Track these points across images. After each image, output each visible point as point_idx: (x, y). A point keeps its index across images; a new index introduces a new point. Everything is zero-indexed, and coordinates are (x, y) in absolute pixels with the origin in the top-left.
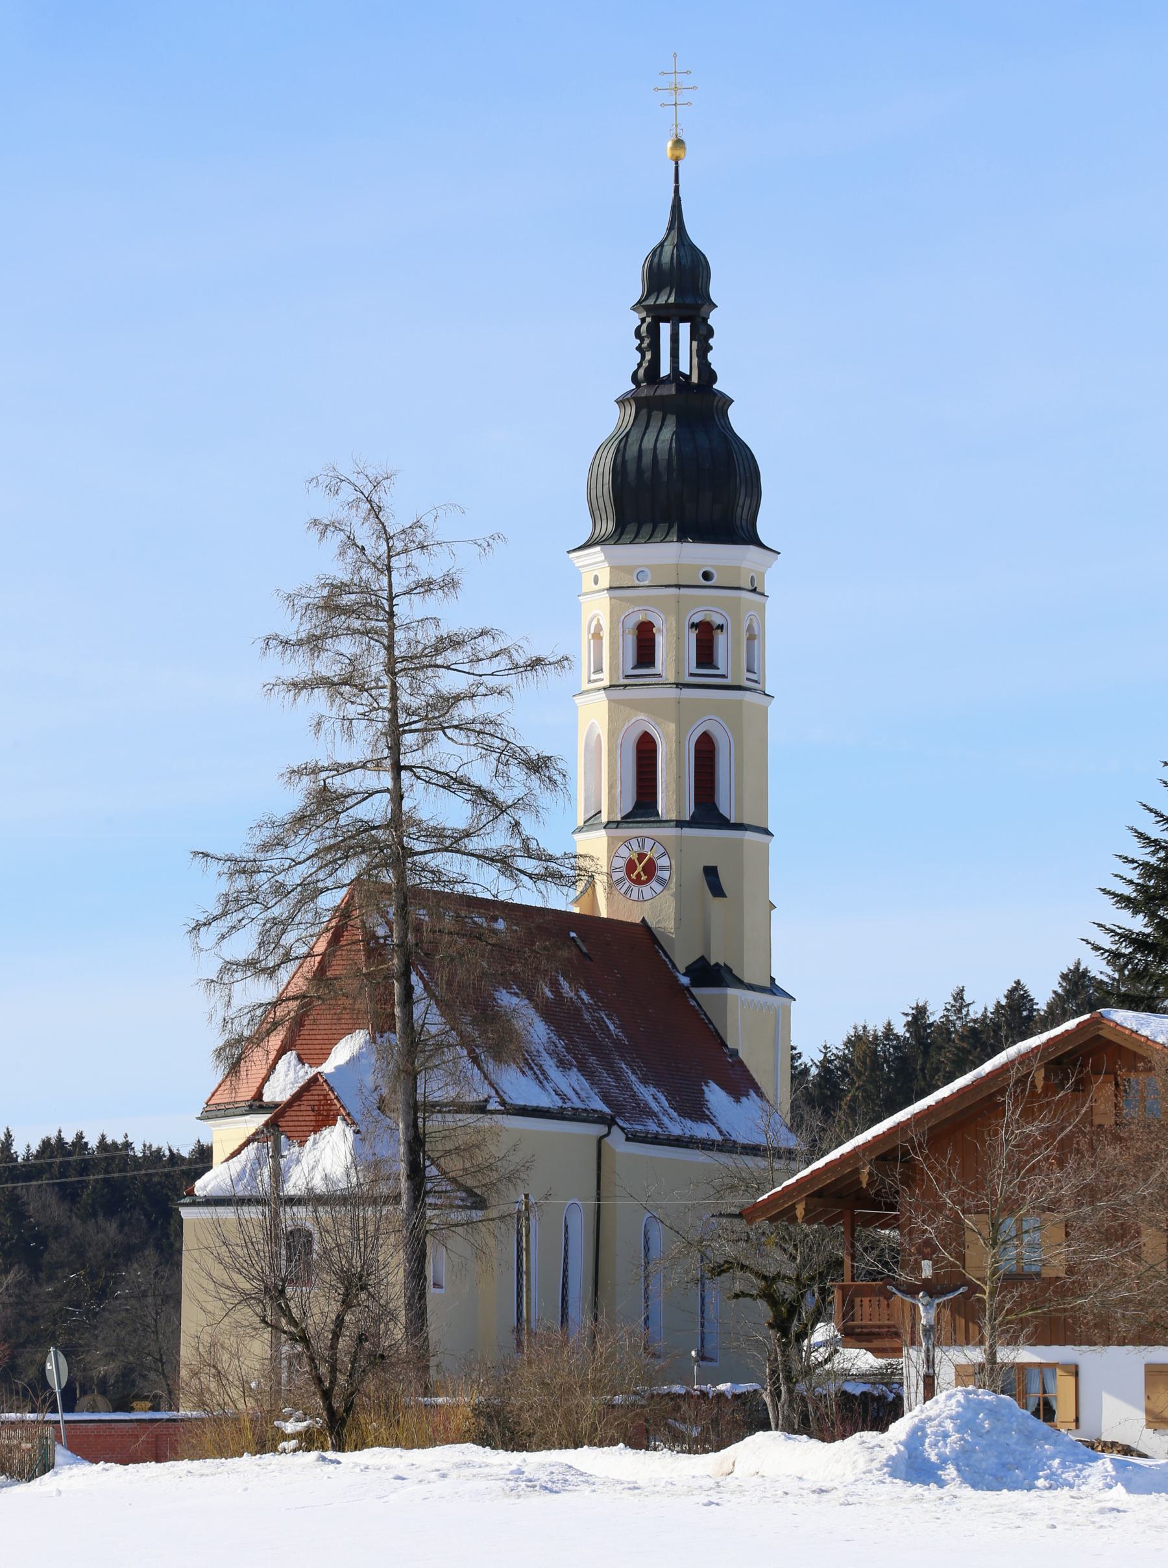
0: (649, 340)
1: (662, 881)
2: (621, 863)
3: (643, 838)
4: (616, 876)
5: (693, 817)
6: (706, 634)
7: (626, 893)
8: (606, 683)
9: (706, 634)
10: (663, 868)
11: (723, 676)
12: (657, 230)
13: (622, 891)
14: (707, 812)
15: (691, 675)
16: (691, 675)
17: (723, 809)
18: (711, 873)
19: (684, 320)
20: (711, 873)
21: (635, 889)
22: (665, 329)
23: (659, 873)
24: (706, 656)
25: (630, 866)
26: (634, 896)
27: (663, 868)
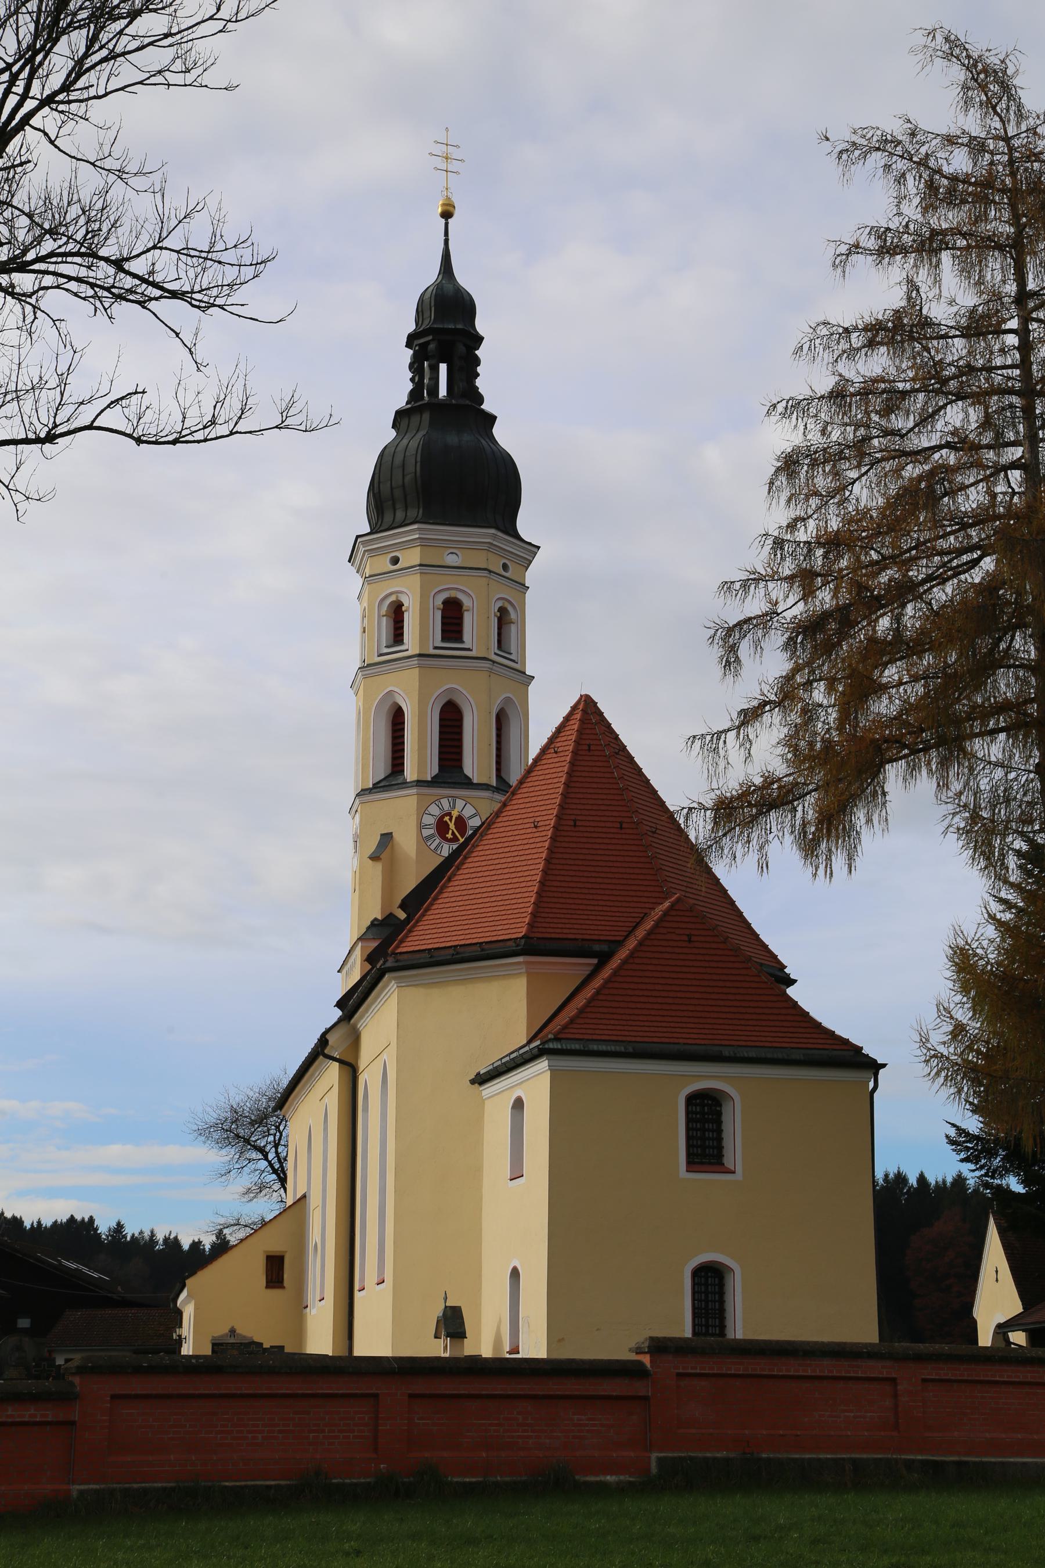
2: (429, 820)
3: (454, 798)
4: (426, 832)
12: (430, 275)
13: (433, 847)
15: (436, 648)
16: (436, 648)
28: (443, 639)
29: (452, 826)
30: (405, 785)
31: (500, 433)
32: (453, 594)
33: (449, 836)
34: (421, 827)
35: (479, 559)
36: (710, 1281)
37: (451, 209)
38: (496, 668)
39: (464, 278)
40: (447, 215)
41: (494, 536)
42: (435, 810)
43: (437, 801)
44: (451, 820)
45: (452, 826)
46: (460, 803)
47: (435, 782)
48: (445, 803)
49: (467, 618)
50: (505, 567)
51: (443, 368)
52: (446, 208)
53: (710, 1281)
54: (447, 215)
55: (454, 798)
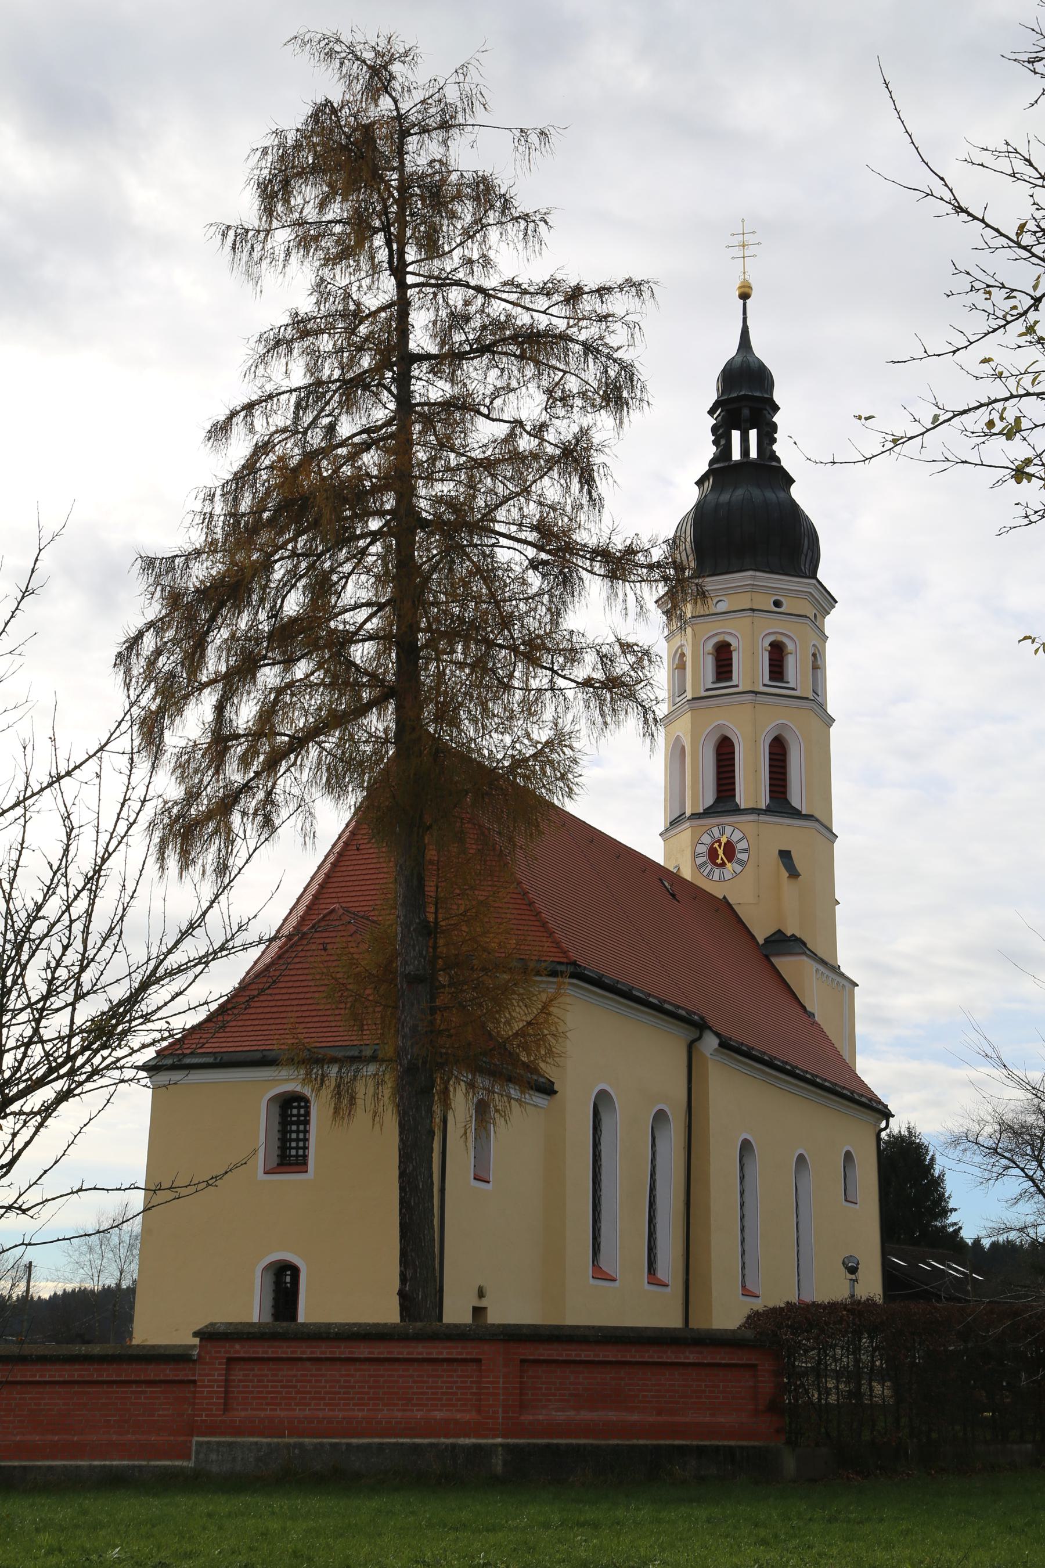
0: (721, 436)
1: (741, 862)
2: (702, 849)
3: (724, 825)
4: (699, 861)
5: (768, 806)
6: (777, 653)
7: (708, 875)
8: (689, 697)
9: (777, 653)
10: (743, 851)
11: (793, 689)
12: (730, 349)
13: (705, 873)
14: (780, 802)
15: (765, 685)
16: (765, 685)
17: (795, 802)
18: (785, 856)
19: (738, 464)
20: (785, 856)
21: (717, 871)
22: (736, 435)
23: (740, 856)
24: (777, 671)
25: (712, 854)
26: (716, 877)
27: (743, 851)
28: (771, 679)
29: (720, 852)
30: (737, 811)
31: (795, 492)
32: (780, 638)
33: (719, 861)
34: (695, 856)
35: (744, 601)
36: (284, 1281)
37: (747, 290)
38: (760, 698)
39: (761, 350)
40: (745, 296)
41: (754, 577)
42: (707, 839)
43: (708, 831)
44: (720, 846)
45: (720, 852)
46: (729, 830)
47: (768, 811)
48: (716, 831)
49: (735, 655)
50: (777, 604)
51: (753, 434)
52: (743, 290)
53: (284, 1281)
54: (745, 296)
55: (724, 825)
